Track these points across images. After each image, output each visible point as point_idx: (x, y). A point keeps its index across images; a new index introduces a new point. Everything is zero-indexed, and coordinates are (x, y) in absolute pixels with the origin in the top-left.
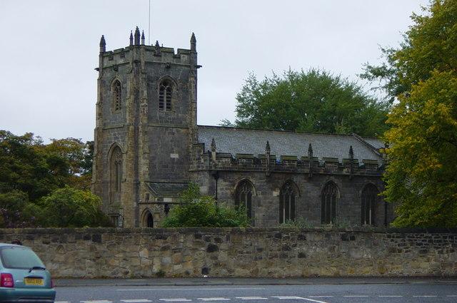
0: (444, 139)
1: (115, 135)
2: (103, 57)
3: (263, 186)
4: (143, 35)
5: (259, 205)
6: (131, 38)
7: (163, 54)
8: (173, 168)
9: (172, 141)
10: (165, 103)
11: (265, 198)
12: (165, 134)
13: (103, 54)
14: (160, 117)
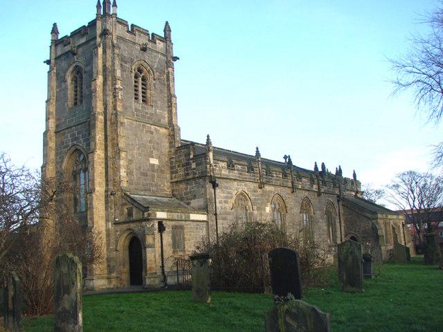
0: (182, 199)
1: (73, 135)
2: (56, 45)
3: (258, 199)
8: (153, 177)
9: (150, 142)
10: (140, 95)
12: (142, 131)
13: (56, 43)
14: (136, 110)
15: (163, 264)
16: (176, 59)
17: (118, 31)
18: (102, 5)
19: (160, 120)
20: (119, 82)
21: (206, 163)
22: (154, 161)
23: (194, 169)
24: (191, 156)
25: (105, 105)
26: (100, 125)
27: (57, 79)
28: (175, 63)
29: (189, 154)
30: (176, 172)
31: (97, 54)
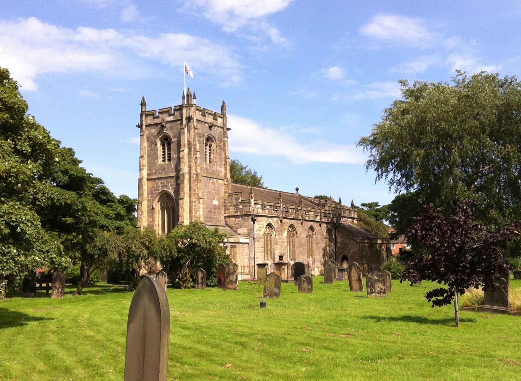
4: (194, 94)
5: (277, 244)
6: (183, 98)
7: (207, 115)
8: (215, 213)
9: (214, 190)
11: (280, 238)
15: (372, 318)
16: (228, 129)
17: (196, 115)
18: (186, 97)
19: (219, 175)
20: (198, 153)
21: (250, 206)
22: (216, 202)
23: (241, 209)
24: (240, 201)
25: (190, 167)
26: (186, 181)
27: (148, 141)
28: (228, 132)
29: (238, 199)
30: (229, 210)
31: (184, 133)
